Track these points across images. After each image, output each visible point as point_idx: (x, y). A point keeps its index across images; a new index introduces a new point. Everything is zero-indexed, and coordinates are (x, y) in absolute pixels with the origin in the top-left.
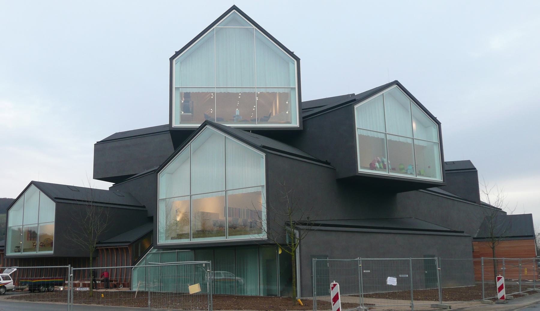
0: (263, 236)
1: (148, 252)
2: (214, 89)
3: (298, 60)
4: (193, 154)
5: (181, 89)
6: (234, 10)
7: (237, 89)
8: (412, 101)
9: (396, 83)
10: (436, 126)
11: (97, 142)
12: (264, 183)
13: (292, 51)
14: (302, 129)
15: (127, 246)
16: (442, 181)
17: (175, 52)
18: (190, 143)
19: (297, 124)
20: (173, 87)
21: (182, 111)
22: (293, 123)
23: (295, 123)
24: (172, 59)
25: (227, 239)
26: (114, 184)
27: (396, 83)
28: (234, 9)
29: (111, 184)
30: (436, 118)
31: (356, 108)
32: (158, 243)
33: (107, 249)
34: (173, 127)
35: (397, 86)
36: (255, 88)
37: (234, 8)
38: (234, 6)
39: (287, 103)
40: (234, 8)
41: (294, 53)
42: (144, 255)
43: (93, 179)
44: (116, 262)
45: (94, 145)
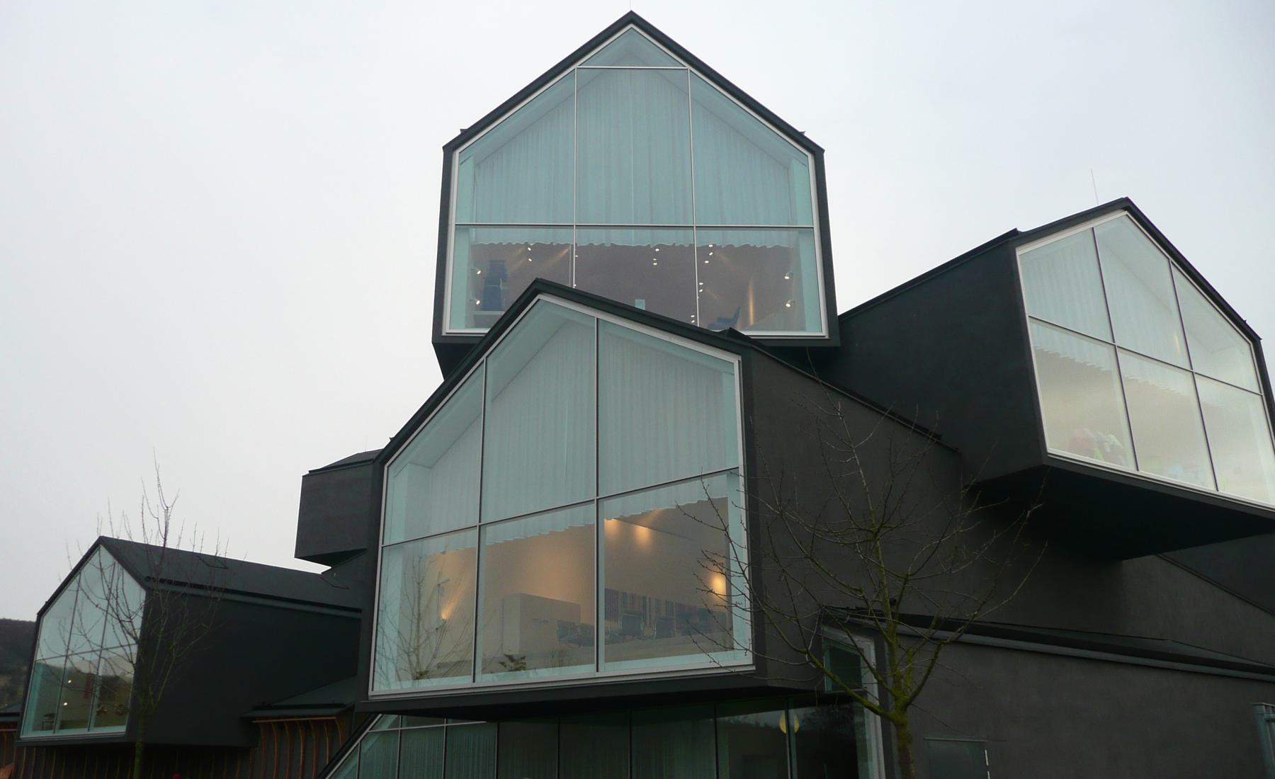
0: (739, 658)
1: (368, 730)
2: (569, 230)
4: (493, 401)
5: (473, 230)
6: (631, 26)
7: (630, 497)
8: (1172, 263)
9: (1125, 205)
11: (310, 471)
12: (737, 459)
13: (800, 130)
14: (839, 344)
15: (334, 718)
17: (461, 130)
18: (484, 358)
20: (450, 223)
21: (475, 299)
24: (450, 149)
25: (598, 675)
32: (370, 693)
33: (281, 726)
35: (1128, 214)
36: (693, 227)
38: (631, 13)
39: (787, 278)
41: (806, 135)
42: (357, 740)
43: (295, 557)
44: (301, 764)
45: (302, 478)
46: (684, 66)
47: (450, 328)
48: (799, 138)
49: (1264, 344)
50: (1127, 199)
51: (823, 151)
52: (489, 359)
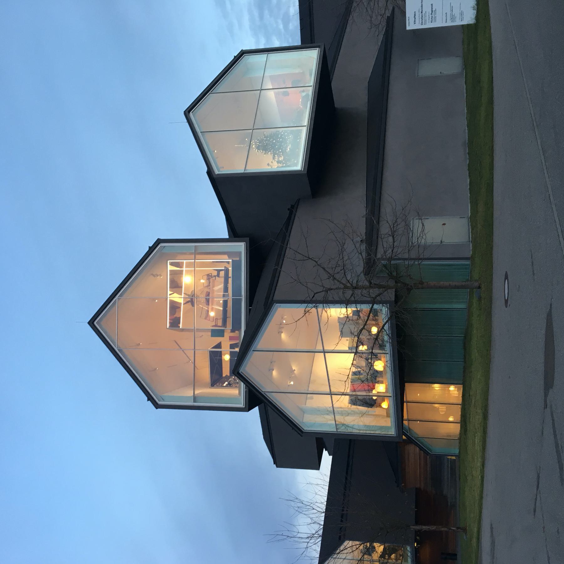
1: (408, 434)
3: (159, 241)
9: (187, 113)
10: (246, 56)
16: (318, 49)
19: (242, 245)
22: (240, 250)
23: (241, 247)
26: (324, 450)
27: (188, 113)
28: (93, 323)
29: (325, 453)
30: (235, 57)
31: (218, 172)
32: (395, 436)
34: (244, 407)
37: (91, 323)
38: (89, 323)
40: (91, 323)
43: (319, 470)
46: (116, 299)
47: (241, 404)
48: (151, 249)
49: (245, 48)
50: (185, 112)
51: (158, 239)
52: (263, 391)
